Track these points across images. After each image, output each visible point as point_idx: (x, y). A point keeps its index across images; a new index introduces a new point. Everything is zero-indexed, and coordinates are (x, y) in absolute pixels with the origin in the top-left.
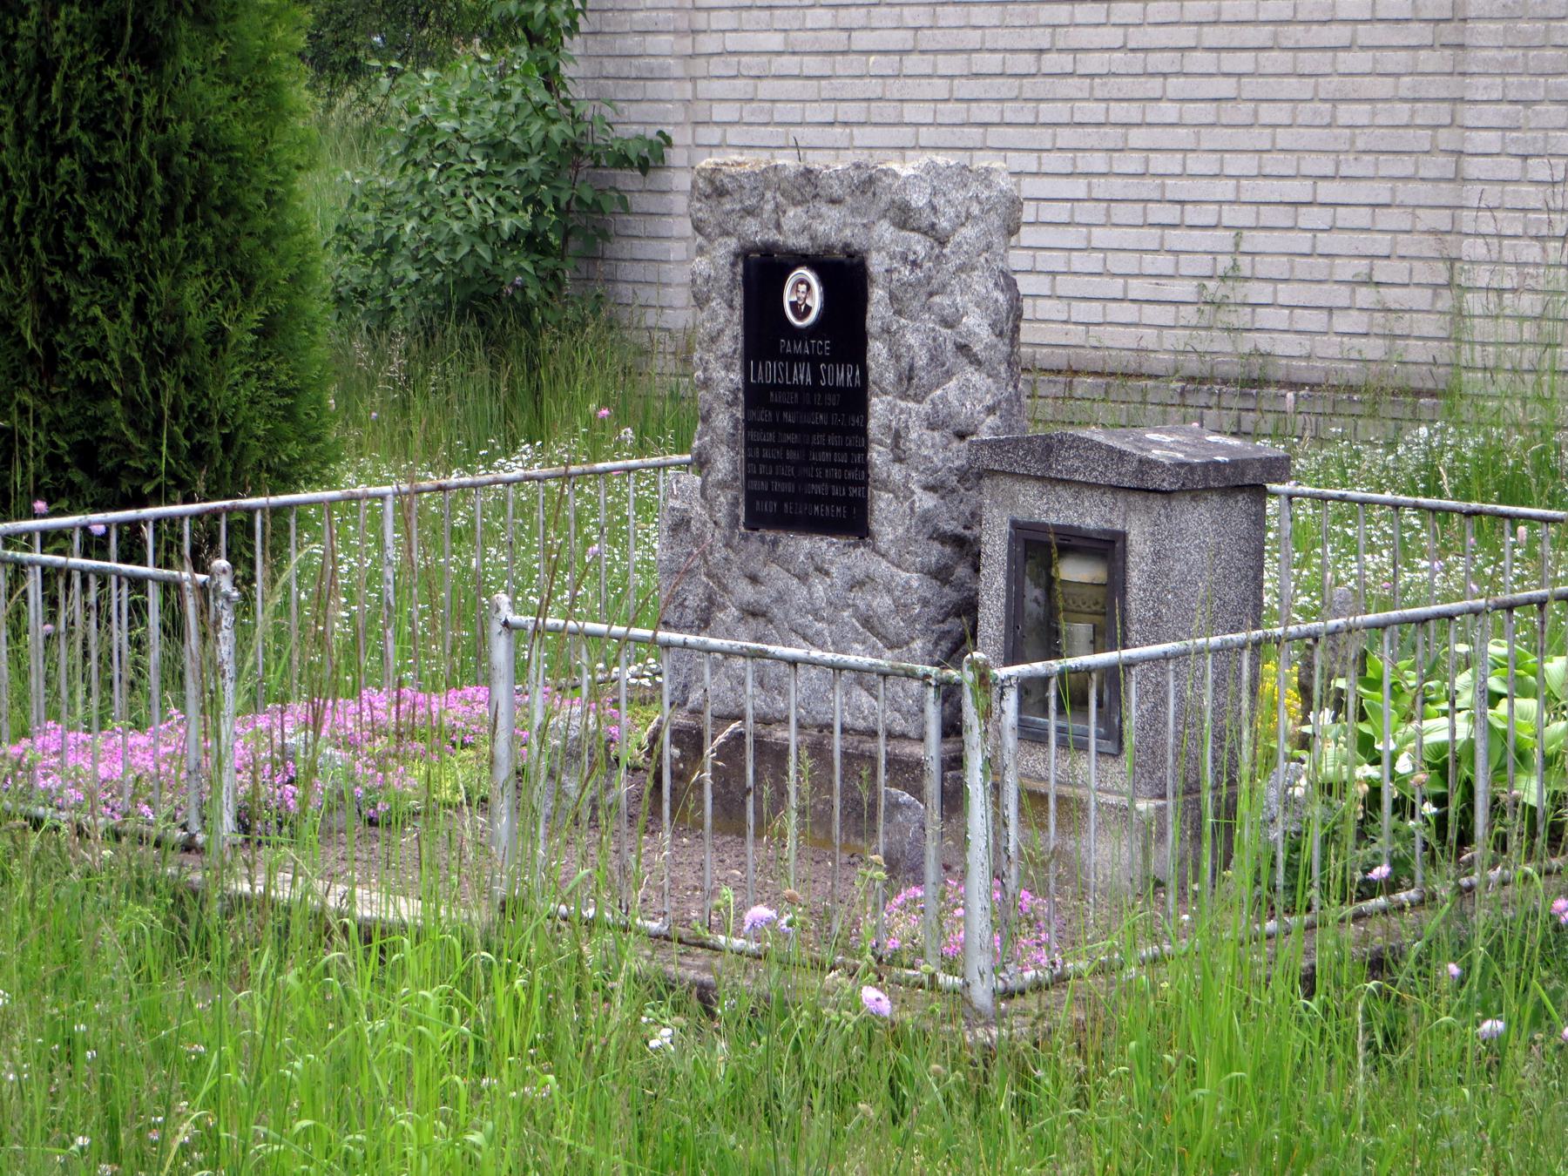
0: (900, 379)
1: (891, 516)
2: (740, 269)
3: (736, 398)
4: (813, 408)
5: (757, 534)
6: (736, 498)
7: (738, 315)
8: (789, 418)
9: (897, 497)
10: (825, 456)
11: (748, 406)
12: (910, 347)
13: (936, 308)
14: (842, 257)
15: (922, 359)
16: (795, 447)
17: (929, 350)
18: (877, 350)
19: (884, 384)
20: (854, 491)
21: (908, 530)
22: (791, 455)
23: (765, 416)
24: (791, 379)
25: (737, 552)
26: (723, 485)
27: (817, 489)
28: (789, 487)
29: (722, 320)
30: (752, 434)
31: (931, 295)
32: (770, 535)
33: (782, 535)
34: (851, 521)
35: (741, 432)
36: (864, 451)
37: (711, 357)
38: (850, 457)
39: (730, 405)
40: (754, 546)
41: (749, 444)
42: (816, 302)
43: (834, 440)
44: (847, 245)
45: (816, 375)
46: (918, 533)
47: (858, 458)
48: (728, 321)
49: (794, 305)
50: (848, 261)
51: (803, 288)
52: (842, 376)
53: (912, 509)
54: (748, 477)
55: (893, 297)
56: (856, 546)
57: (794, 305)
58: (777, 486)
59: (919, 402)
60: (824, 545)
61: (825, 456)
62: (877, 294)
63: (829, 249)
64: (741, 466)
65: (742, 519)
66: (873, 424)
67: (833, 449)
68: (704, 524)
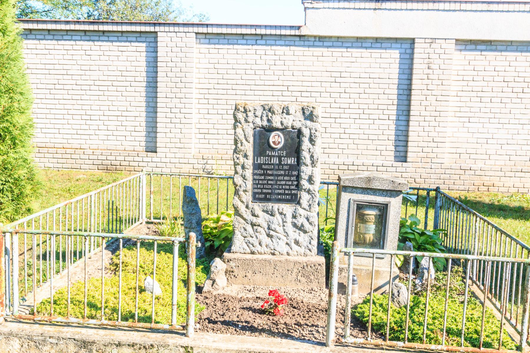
10: (284, 183)
28: (270, 191)
43: (286, 178)
45: (280, 161)
57: (274, 142)
58: (264, 191)
61: (284, 183)
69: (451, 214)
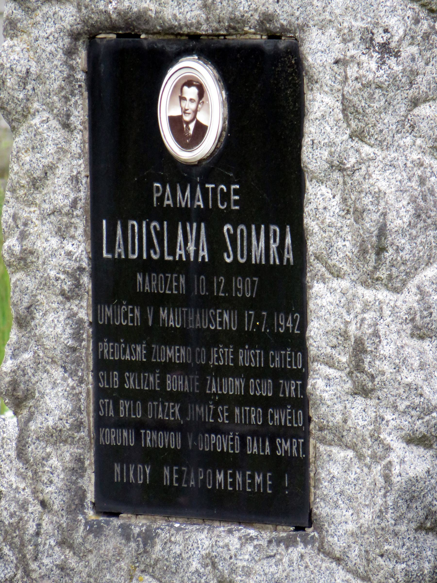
0: (364, 251)
1: (349, 491)
2: (81, 59)
3: (78, 285)
4: (210, 302)
5: (116, 522)
6: (79, 460)
7: (79, 141)
8: (170, 318)
9: (360, 457)
10: (234, 386)
11: (100, 298)
12: (378, 196)
13: (424, 126)
14: (259, 39)
15: (400, 217)
16: (184, 369)
17: (413, 200)
18: (321, 201)
19: (335, 260)
20: (284, 446)
21: (381, 515)
22: (175, 383)
23: (128, 315)
24: (172, 252)
25: (82, 556)
26: (55, 437)
27: (222, 443)
28: (172, 440)
29: (51, 149)
30: (106, 347)
31: (415, 103)
32: (139, 524)
33: (160, 522)
34: (280, 497)
35: (87, 344)
36: (302, 375)
37: (30, 213)
38: (276, 387)
39: (67, 297)
40: (111, 543)
41: (101, 365)
42: (214, 115)
43: (248, 357)
44: (267, 18)
45: (216, 244)
46: (398, 520)
47: (291, 388)
48: (62, 151)
49: (176, 123)
50: (269, 46)
51: (191, 92)
52: (261, 246)
53: (387, 478)
54: (101, 422)
55: (348, 109)
56: (289, 543)
57: (176, 123)
58: (150, 438)
59: (396, 291)
60: (234, 541)
61: (234, 386)
62: (321, 106)
63: (236, 24)
64: (87, 404)
65: (91, 496)
66: (318, 333)
67: (249, 373)
68: (24, 506)
69: (191, 407)
